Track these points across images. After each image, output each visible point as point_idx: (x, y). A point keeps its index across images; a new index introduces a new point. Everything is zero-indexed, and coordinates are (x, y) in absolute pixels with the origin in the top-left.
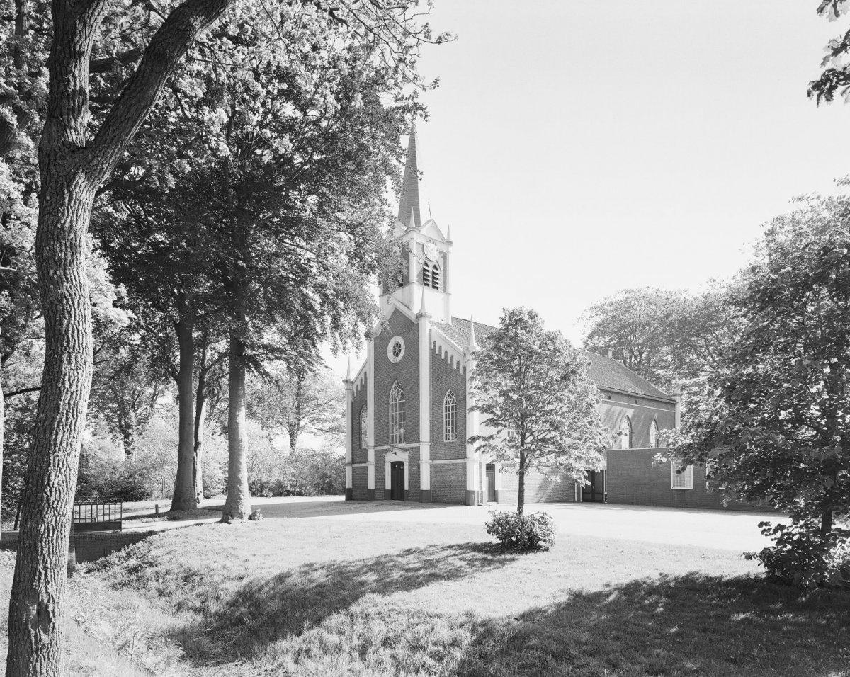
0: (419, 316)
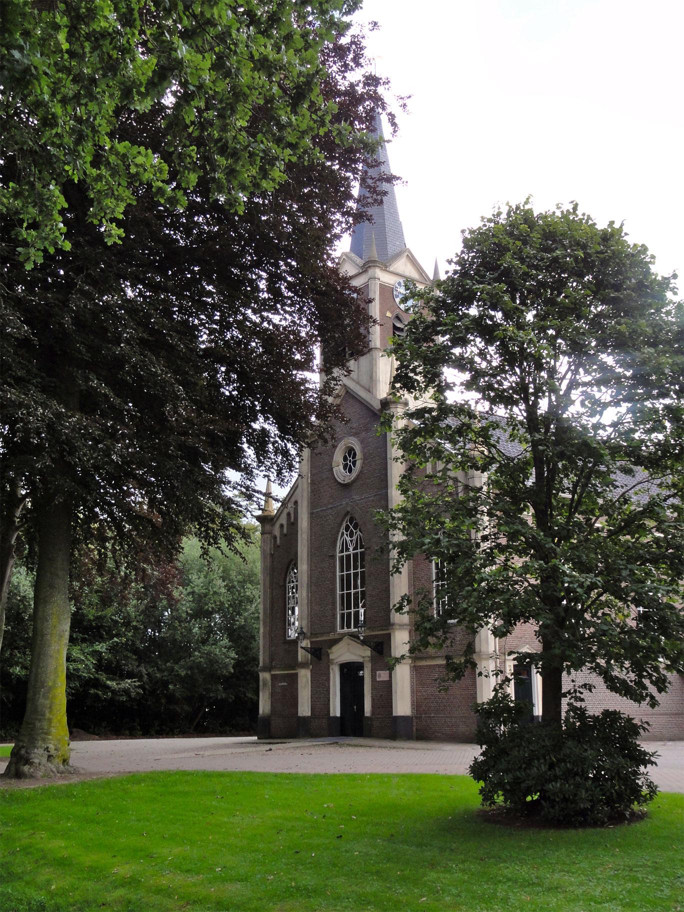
0: (182, 58)
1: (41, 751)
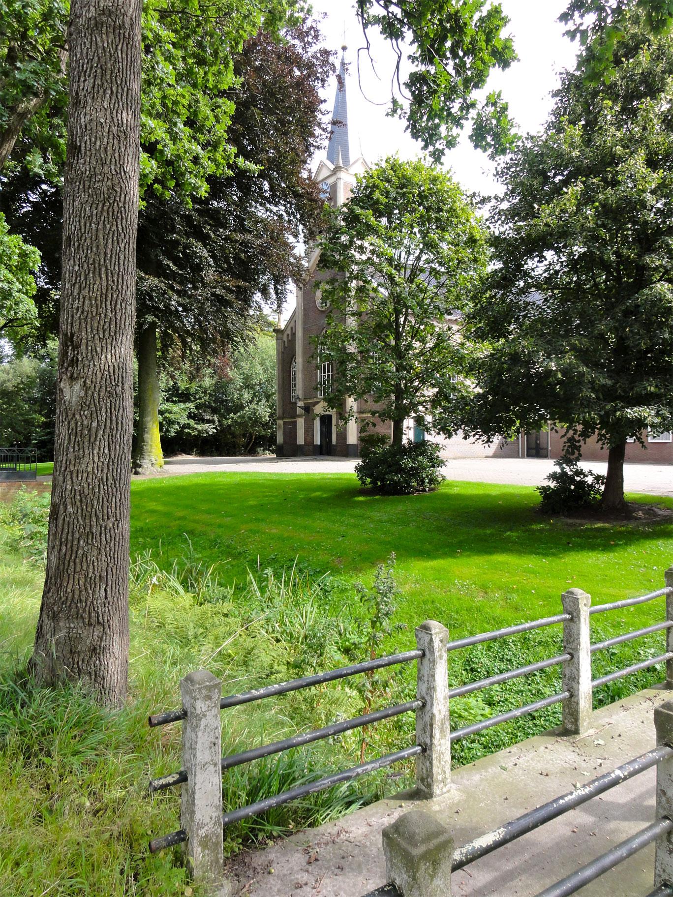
1: (147, 461)
